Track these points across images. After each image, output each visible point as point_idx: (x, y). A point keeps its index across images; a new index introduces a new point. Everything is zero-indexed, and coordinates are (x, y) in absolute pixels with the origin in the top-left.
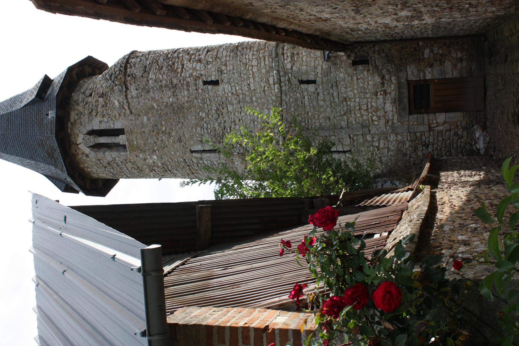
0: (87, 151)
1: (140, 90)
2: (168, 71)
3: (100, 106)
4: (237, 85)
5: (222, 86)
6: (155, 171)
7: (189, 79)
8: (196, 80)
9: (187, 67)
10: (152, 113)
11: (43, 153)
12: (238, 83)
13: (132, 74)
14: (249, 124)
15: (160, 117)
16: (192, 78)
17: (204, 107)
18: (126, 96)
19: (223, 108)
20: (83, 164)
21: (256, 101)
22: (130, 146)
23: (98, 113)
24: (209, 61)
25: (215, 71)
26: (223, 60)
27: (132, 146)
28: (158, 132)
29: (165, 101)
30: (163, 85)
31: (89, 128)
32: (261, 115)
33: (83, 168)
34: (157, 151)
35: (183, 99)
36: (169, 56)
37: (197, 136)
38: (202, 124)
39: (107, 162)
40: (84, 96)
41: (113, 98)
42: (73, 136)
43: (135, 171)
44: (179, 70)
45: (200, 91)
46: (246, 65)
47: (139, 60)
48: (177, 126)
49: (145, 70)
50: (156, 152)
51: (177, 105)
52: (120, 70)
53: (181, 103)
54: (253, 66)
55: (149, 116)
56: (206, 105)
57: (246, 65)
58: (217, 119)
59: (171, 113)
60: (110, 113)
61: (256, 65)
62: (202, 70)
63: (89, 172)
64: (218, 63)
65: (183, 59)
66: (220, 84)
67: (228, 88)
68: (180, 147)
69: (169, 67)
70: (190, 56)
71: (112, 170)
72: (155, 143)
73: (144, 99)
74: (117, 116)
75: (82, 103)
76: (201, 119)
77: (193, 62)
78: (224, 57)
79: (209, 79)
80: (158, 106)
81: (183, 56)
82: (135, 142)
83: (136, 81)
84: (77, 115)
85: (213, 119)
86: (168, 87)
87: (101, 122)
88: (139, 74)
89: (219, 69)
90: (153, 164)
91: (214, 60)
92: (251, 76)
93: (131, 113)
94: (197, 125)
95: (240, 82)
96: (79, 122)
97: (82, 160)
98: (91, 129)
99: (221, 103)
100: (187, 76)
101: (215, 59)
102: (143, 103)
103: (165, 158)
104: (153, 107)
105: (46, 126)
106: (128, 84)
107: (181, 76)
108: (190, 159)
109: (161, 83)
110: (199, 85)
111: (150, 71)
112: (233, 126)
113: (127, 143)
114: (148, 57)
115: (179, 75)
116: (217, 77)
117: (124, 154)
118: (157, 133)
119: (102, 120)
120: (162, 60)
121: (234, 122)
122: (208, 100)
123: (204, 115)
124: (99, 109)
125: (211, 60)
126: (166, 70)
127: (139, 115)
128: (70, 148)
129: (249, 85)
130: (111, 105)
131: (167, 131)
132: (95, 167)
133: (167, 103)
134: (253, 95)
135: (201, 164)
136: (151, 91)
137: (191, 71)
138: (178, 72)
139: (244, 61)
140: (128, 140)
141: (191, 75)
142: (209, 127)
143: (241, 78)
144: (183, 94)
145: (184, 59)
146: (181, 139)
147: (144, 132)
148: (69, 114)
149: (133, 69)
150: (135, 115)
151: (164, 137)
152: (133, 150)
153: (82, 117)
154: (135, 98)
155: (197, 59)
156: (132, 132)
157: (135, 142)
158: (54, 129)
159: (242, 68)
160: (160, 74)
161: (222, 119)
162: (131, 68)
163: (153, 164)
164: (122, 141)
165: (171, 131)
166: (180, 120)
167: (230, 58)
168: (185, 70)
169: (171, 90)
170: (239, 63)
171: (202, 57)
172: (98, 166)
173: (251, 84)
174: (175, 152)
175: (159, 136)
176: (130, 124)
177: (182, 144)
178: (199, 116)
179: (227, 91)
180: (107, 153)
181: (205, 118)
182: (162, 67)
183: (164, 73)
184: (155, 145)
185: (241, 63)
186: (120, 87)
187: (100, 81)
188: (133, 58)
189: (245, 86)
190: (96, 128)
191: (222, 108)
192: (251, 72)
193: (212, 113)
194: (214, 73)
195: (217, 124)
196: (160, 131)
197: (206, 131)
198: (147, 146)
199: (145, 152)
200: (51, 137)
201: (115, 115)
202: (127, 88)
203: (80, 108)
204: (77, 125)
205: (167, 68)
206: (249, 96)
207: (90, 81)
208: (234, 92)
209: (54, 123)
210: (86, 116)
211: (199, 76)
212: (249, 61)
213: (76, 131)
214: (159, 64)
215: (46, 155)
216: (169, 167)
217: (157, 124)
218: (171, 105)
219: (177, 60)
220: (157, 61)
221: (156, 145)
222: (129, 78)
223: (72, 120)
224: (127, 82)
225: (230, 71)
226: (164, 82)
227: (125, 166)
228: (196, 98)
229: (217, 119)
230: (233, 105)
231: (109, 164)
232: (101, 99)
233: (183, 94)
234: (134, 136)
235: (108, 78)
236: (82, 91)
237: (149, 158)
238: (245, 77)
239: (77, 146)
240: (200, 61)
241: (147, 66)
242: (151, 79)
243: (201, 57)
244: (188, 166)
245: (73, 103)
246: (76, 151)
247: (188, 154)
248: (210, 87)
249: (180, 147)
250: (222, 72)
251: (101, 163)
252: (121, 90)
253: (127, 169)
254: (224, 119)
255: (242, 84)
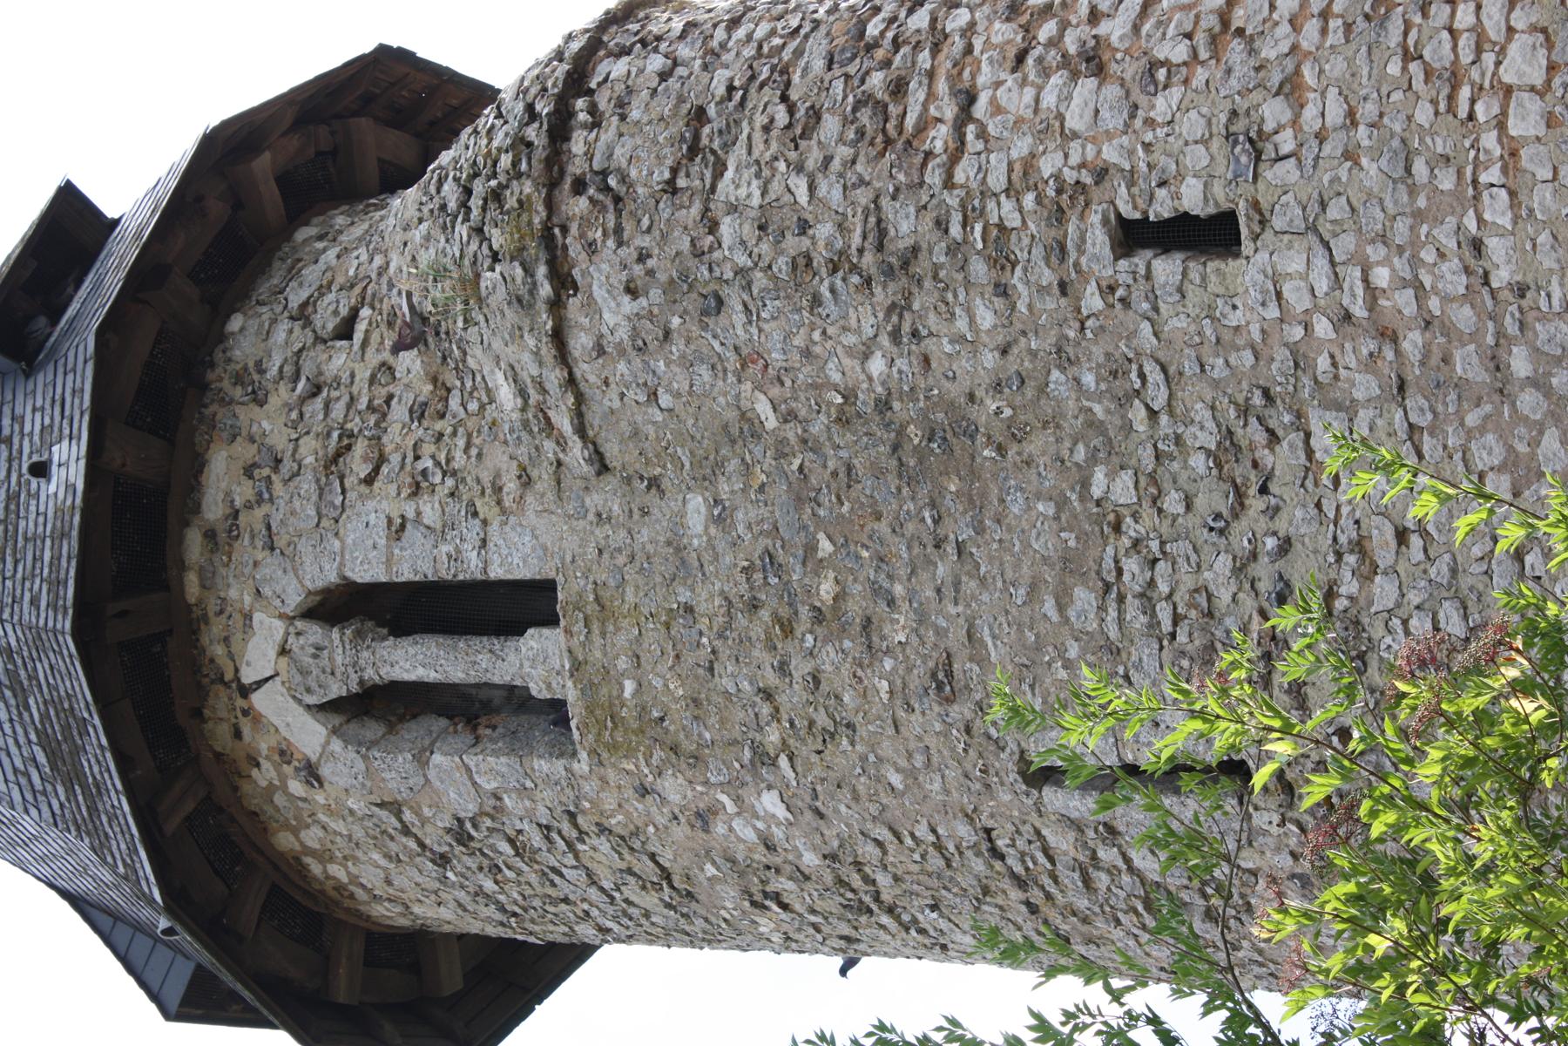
0: (309, 735)
1: (656, 294)
2: (854, 144)
3: (399, 412)
4: (1375, 252)
5: (1262, 257)
6: (785, 907)
7: (1008, 205)
8: (1059, 216)
9: (997, 109)
10: (747, 468)
11: (22, 740)
12: (1383, 238)
13: (604, 173)
14: (1478, 568)
15: (799, 501)
16: (1029, 200)
17: (1128, 428)
18: (559, 338)
19: (1273, 438)
20: (296, 832)
21: (1538, 383)
22: (590, 710)
23: (382, 459)
24: (1165, 63)
25: (1204, 142)
26: (1268, 52)
27: (606, 714)
28: (784, 612)
29: (836, 377)
30: (820, 257)
31: (321, 573)
32: (1473, 518)
33: (297, 859)
34: (783, 761)
35: (963, 365)
36: (873, 30)
37: (1073, 651)
38: (1108, 563)
39: (446, 821)
40: (301, 337)
41: (478, 351)
42: (217, 628)
43: (650, 900)
44: (939, 138)
45: (1092, 301)
46: (1455, 79)
47: (656, 62)
48: (924, 576)
49: (697, 137)
50: (774, 763)
51: (924, 414)
52: (520, 144)
53: (955, 391)
54: (1509, 90)
55: (724, 488)
56: (1138, 414)
57: (1455, 88)
58: (1221, 527)
59: (878, 473)
60: (459, 460)
61: (1538, 79)
62: (1109, 136)
63: (340, 888)
64: (1229, 71)
65: (969, 50)
66: (1247, 246)
67: (1304, 277)
68: (946, 734)
69: (865, 116)
70: (1026, 29)
71: (489, 885)
72: (767, 694)
73: (688, 364)
74: (511, 486)
75: (283, 388)
76: (1098, 520)
77: (1046, 73)
78: (1285, 28)
79: (1162, 208)
80: (789, 417)
81: (972, 25)
82: (629, 687)
83: (628, 227)
84: (249, 471)
85: (1192, 521)
86: (854, 268)
87: (398, 529)
88: (648, 173)
89: (1239, 126)
90: (761, 856)
91: (1204, 54)
92: (1492, 175)
93: (603, 468)
94: (1069, 564)
95: (1402, 227)
96: (260, 527)
97: (279, 799)
98: (332, 577)
99: (1257, 400)
100: (997, 181)
101: (1214, 40)
102: (678, 395)
103: (844, 817)
104: (750, 427)
105: (30, 546)
106: (575, 249)
107: (949, 184)
108: (1026, 829)
109: (805, 243)
110: (1081, 250)
111: (727, 147)
112: (1349, 586)
113: (571, 694)
114: (723, 46)
115: (934, 177)
116: (1218, 190)
117: (559, 765)
118: (777, 619)
119: (411, 514)
120: (819, 64)
121: (1360, 546)
122: (1154, 375)
123: (1123, 490)
124: (394, 436)
125: (1179, 53)
126: (841, 140)
127: (654, 483)
128: (198, 713)
129: (1477, 246)
130: (473, 406)
131: (855, 608)
132: (376, 856)
133: (849, 396)
134: (1511, 328)
135: (1112, 871)
136: (734, 299)
137: (1021, 147)
138: (929, 155)
139: (1438, 51)
140: (577, 667)
141: (1024, 175)
142: (1164, 588)
143: (1413, 191)
144: (962, 324)
145: (978, 47)
146: (949, 674)
147: (689, 609)
148: (198, 465)
149: (607, 135)
150: (628, 480)
151: (829, 656)
152: (613, 747)
153: (278, 487)
154: (622, 352)
155: (1072, 49)
156: (603, 611)
157: (629, 687)
158: (72, 573)
159: (1423, 115)
160: (800, 169)
161: (1262, 524)
162: (596, 124)
163: (761, 856)
164: (540, 671)
165: (883, 606)
166: (948, 529)
167: (1324, 31)
168: (982, 134)
169: (878, 290)
170: (1394, 68)
171: (1115, 29)
172: (393, 847)
173: (1493, 243)
174: (910, 774)
175: (790, 647)
176: (592, 552)
177: (961, 711)
178: (1085, 495)
179: (1297, 299)
180: (437, 758)
181: (1136, 517)
182: (815, 114)
183: (828, 160)
184: (766, 710)
185: (1414, 67)
186: (519, 271)
187: (406, 228)
188: (625, 51)
189: (1441, 255)
190: (368, 571)
191: (1260, 437)
192: (1490, 140)
193: (1183, 477)
194: (1197, 157)
195: (1223, 564)
196: (804, 611)
197: (1136, 617)
198: (713, 720)
199: (697, 759)
200: (54, 630)
201: (498, 475)
202: (563, 282)
203: (270, 423)
204: (247, 550)
205: (846, 122)
206: (1475, 336)
207: (358, 231)
208: (1359, 311)
209: (75, 533)
210: (307, 484)
211: (1087, 179)
212: (1479, 50)
213: (238, 593)
214: (794, 95)
215: (41, 758)
216: (883, 880)
217: (780, 555)
218: (883, 405)
219: (924, 59)
220: (785, 71)
221: (776, 715)
222: (582, 203)
223: (213, 509)
224: (565, 230)
225: (1321, 137)
226: (824, 230)
227: (570, 860)
228: (1063, 357)
229: (1221, 527)
230: (1349, 409)
231: (463, 838)
232: (409, 361)
233: (962, 324)
234: (621, 640)
235: (452, 205)
236: (296, 297)
237: (731, 807)
238: (1446, 182)
239: (240, 703)
240: (1094, 61)
241: (712, 111)
242: (733, 209)
243: (1103, 28)
244: (1021, 883)
245: (226, 384)
246: (238, 734)
247: (1008, 797)
248: (1167, 268)
249: (946, 734)
250: (1257, 145)
251: (406, 831)
252: (523, 291)
253: (593, 880)
254: (1281, 525)
255: (1415, 243)
